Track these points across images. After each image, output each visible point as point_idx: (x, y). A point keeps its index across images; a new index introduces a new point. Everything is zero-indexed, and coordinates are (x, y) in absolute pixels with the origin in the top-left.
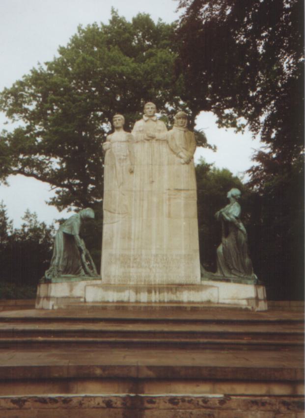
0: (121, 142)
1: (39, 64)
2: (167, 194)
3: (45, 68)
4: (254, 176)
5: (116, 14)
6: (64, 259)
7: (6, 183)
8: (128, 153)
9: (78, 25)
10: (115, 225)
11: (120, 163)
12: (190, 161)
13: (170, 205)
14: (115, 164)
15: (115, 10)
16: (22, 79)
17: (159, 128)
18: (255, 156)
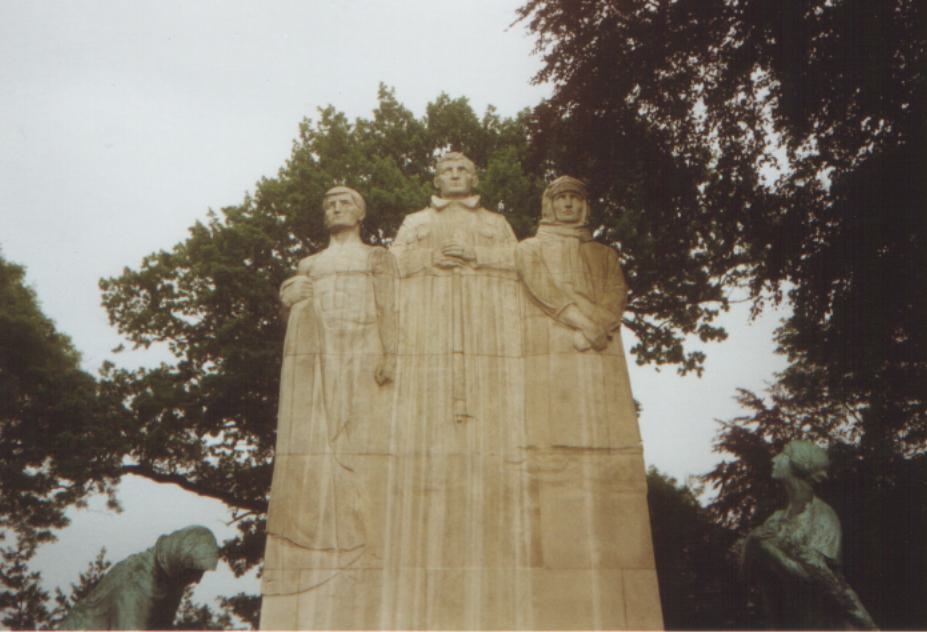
0: (348, 273)
1: (211, 213)
2: (524, 466)
3: (222, 219)
4: (725, 488)
5: (391, 98)
7: (113, 504)
8: (373, 312)
9: (301, 120)
11: (342, 349)
12: (610, 338)
13: (537, 512)
14: (322, 353)
15: (388, 90)
16: (170, 250)
17: (488, 231)
18: (718, 442)
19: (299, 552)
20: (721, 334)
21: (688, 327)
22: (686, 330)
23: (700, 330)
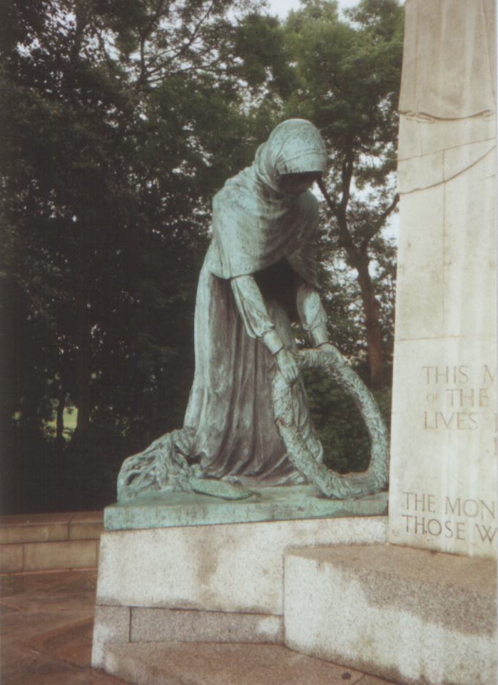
19: (443, 127)
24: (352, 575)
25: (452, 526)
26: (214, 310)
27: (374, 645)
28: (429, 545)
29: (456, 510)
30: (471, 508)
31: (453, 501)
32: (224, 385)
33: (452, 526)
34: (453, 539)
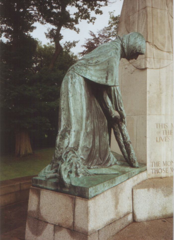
6: (87, 134)
10: (164, 70)
19: (159, 52)
20: (101, 13)
21: (92, 9)
22: (91, 10)
23: (96, 10)
24: (159, 190)
25: (165, 170)
26: (86, 96)
27: (166, 209)
28: (159, 176)
29: (166, 165)
30: (169, 164)
31: (165, 162)
32: (90, 129)
33: (165, 170)
34: (165, 173)
